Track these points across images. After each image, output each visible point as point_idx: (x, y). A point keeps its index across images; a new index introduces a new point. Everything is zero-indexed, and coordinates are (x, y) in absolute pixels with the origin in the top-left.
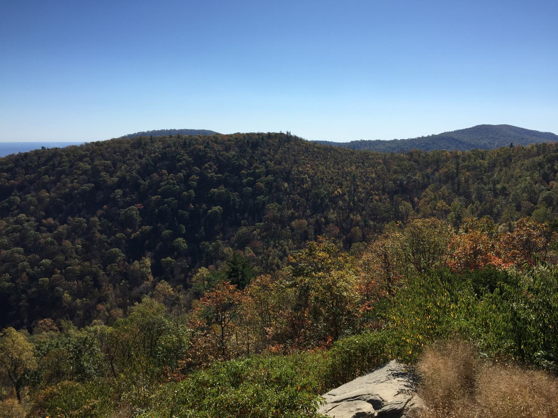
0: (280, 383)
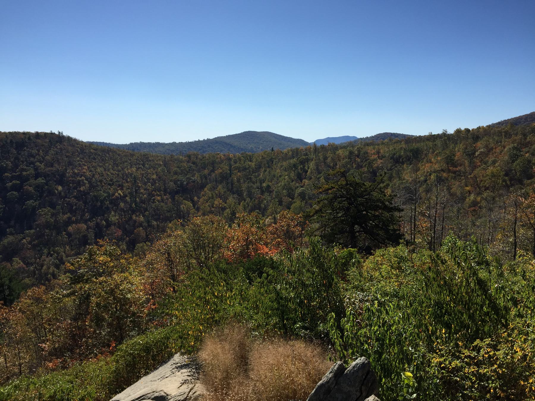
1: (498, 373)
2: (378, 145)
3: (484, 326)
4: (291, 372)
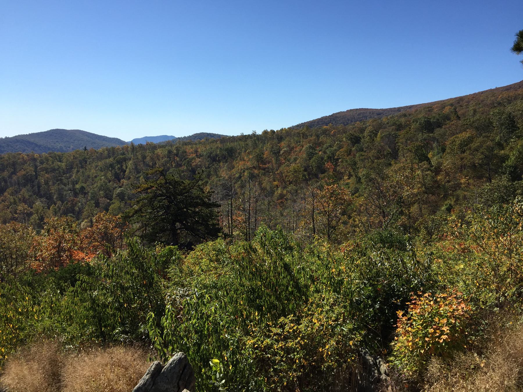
1: (301, 345)
2: (196, 144)
3: (289, 304)
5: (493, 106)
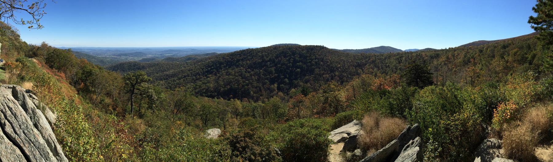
0: (317, 128)
4: (393, 129)
5: (524, 41)
